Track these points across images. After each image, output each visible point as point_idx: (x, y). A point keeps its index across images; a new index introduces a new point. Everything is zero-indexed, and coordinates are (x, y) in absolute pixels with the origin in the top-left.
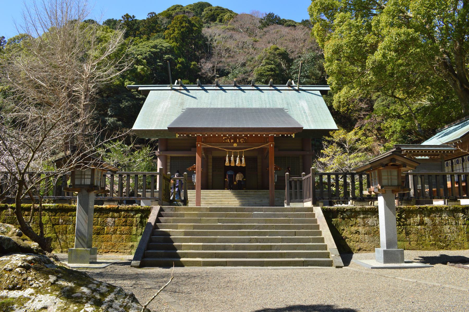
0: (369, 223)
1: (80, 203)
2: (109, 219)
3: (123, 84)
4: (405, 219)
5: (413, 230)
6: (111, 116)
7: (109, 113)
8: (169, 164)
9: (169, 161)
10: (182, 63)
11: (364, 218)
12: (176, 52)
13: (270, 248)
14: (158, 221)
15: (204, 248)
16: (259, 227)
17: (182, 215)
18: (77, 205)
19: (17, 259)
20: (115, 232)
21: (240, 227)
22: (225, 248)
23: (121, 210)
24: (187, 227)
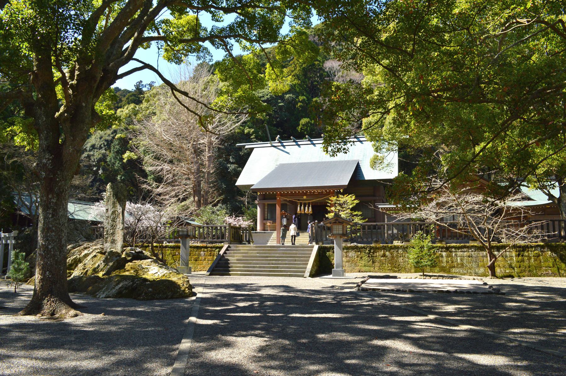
0: (350, 255)
1: (336, 244)
2: (202, 252)
3: (243, 131)
4: (373, 253)
5: (378, 260)
6: (232, 163)
7: (231, 160)
8: (266, 210)
9: (266, 207)
10: (303, 101)
11: (346, 252)
12: (298, 90)
13: (278, 267)
14: (225, 253)
15: (244, 267)
16: (277, 257)
17: (239, 250)
18: (181, 245)
19: (150, 260)
20: (205, 260)
21: (267, 257)
22: (254, 267)
23: (208, 247)
24: (239, 256)
